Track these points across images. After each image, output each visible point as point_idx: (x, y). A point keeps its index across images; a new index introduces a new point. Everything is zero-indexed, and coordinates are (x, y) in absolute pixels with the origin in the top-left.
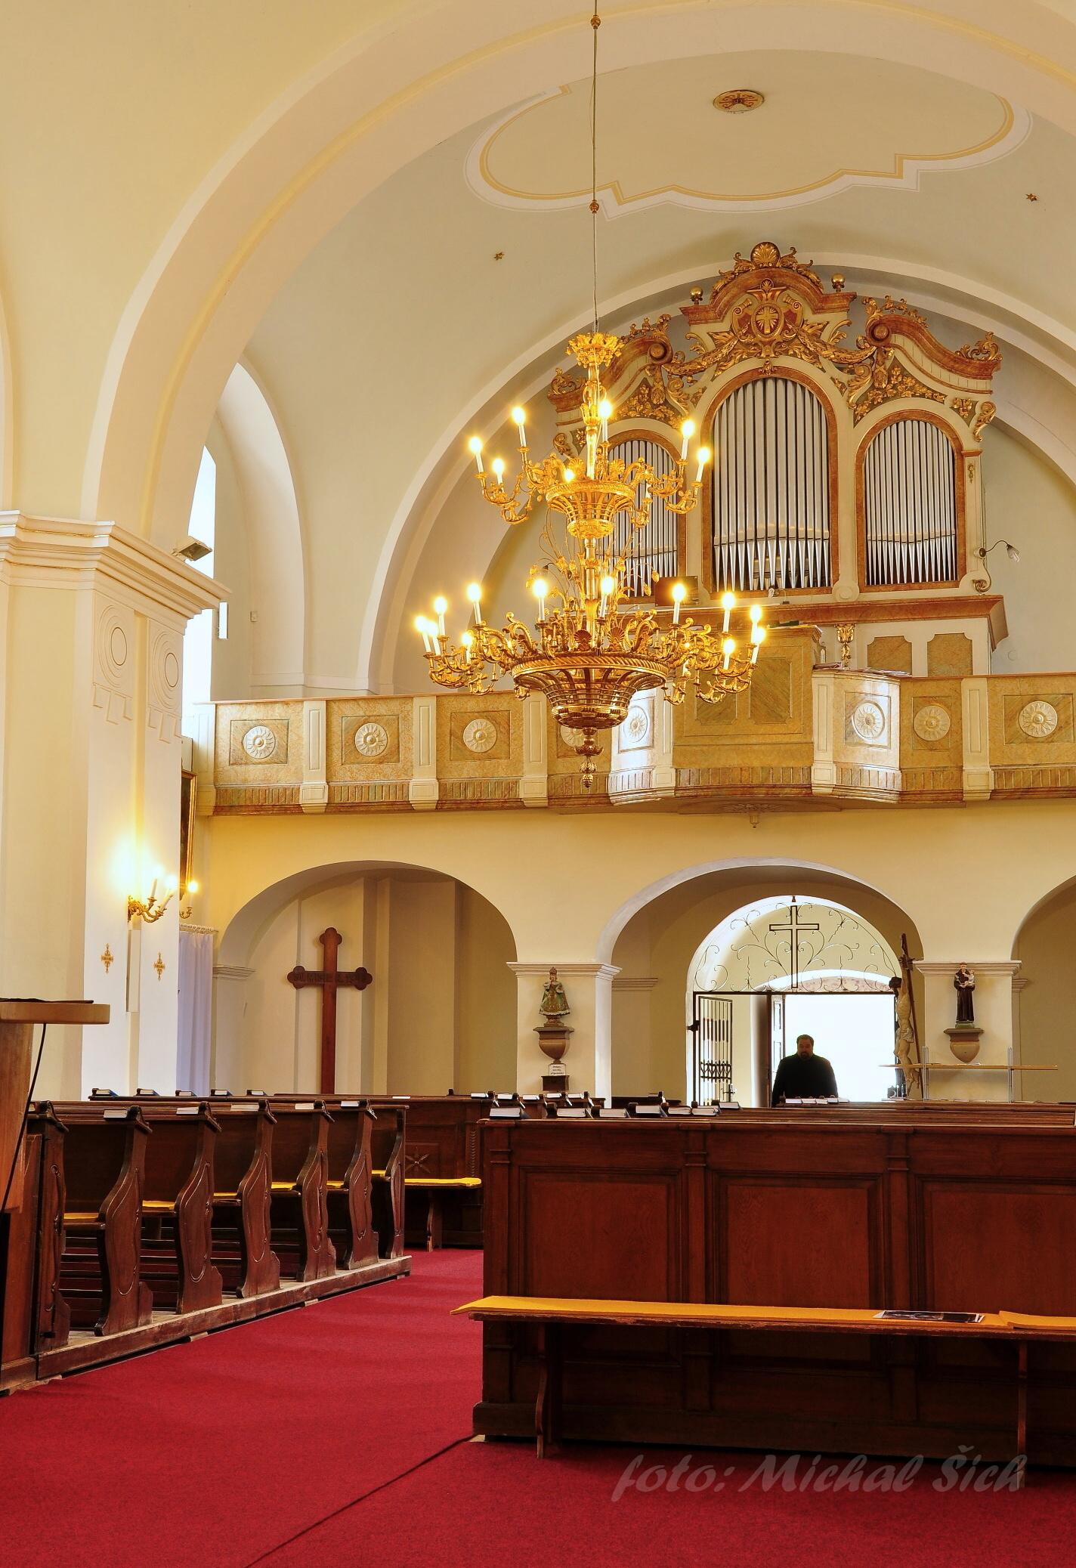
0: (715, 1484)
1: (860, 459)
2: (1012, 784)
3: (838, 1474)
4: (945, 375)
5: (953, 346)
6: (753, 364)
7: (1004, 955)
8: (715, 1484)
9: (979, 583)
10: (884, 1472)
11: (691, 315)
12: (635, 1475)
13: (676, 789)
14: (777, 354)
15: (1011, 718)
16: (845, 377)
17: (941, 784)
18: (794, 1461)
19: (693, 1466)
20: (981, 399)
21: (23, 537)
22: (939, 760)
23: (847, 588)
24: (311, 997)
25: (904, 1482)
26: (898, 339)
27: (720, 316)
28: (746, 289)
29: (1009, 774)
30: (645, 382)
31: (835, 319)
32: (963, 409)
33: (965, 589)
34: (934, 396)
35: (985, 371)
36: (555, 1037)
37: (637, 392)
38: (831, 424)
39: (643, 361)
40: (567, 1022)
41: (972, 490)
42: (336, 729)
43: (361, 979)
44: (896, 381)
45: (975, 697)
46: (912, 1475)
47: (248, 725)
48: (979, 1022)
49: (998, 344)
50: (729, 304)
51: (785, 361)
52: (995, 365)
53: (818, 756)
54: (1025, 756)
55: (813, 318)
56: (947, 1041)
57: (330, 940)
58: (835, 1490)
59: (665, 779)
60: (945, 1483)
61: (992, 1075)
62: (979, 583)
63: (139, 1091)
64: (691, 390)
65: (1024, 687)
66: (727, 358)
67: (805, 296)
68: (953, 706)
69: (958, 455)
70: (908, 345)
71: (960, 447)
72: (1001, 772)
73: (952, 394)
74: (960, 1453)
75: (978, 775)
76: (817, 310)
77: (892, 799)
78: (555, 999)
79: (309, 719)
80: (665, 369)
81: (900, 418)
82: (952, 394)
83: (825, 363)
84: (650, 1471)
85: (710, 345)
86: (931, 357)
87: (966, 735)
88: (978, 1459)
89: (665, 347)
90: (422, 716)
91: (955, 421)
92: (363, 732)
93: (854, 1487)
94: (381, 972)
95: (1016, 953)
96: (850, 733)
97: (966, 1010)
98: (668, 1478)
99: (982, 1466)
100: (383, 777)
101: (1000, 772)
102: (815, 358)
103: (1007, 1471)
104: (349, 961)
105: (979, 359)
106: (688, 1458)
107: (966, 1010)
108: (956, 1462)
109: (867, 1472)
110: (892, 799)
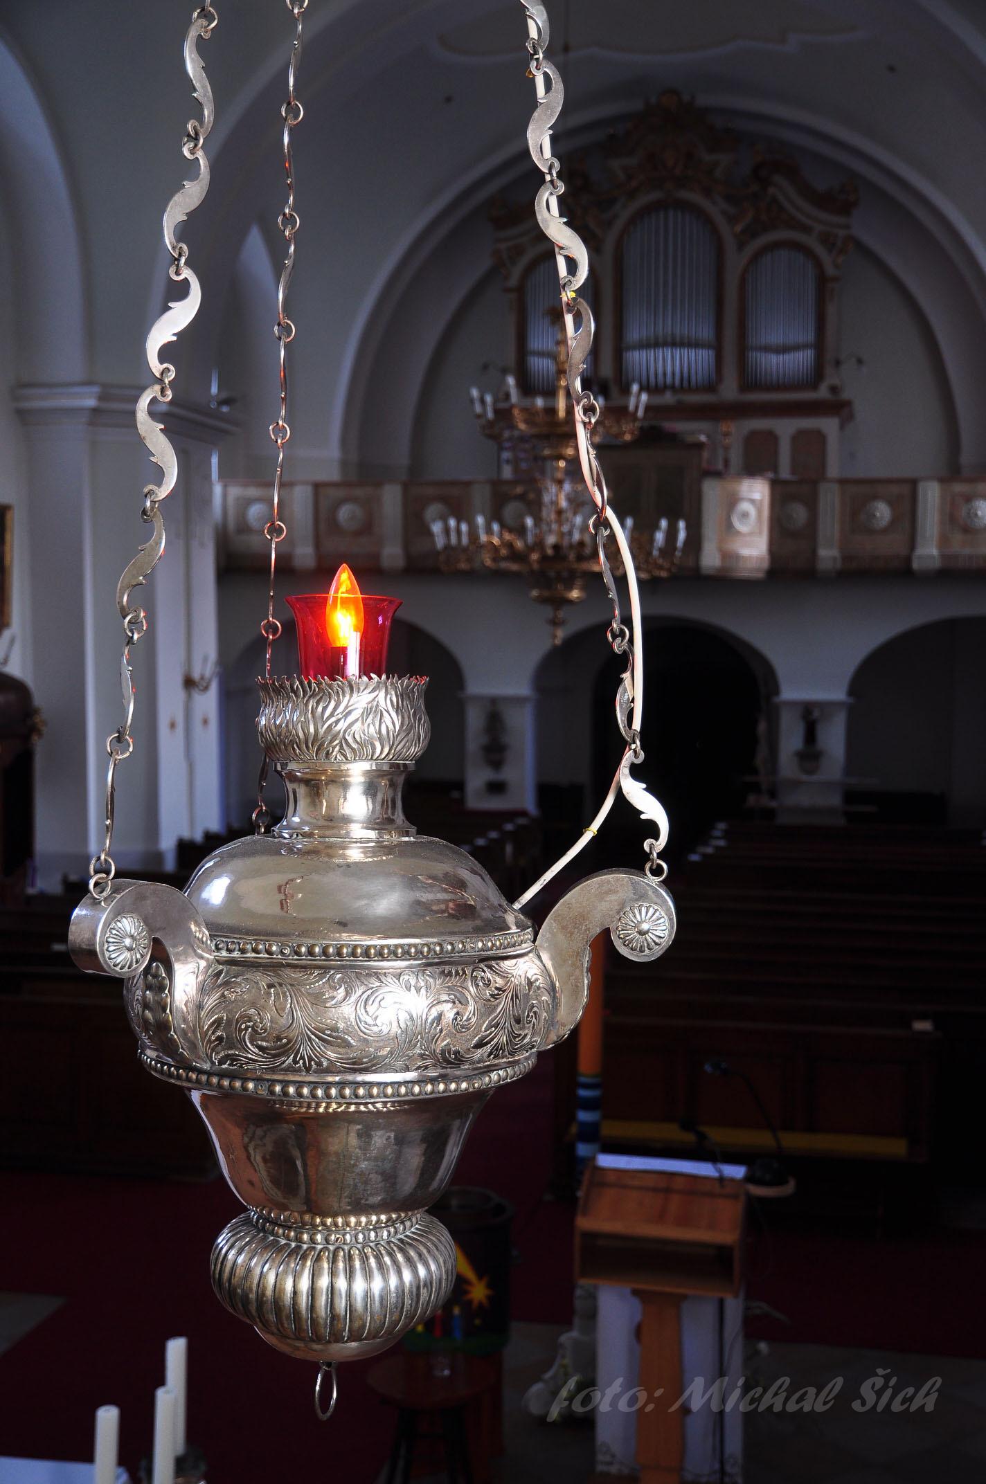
3: (765, 1391)
6: (655, 196)
9: (834, 389)
10: (806, 1393)
21: (105, 405)
25: (825, 1403)
32: (827, 240)
33: (823, 393)
36: (495, 752)
41: (831, 310)
45: (830, 500)
47: (249, 502)
51: (686, 195)
60: (863, 1403)
62: (834, 389)
68: (812, 504)
72: (846, 558)
75: (828, 554)
78: (494, 722)
79: (301, 497)
88: (893, 1381)
90: (391, 499)
91: (820, 250)
93: (777, 1408)
95: (851, 692)
96: (730, 526)
100: (890, 546)
105: (842, 198)
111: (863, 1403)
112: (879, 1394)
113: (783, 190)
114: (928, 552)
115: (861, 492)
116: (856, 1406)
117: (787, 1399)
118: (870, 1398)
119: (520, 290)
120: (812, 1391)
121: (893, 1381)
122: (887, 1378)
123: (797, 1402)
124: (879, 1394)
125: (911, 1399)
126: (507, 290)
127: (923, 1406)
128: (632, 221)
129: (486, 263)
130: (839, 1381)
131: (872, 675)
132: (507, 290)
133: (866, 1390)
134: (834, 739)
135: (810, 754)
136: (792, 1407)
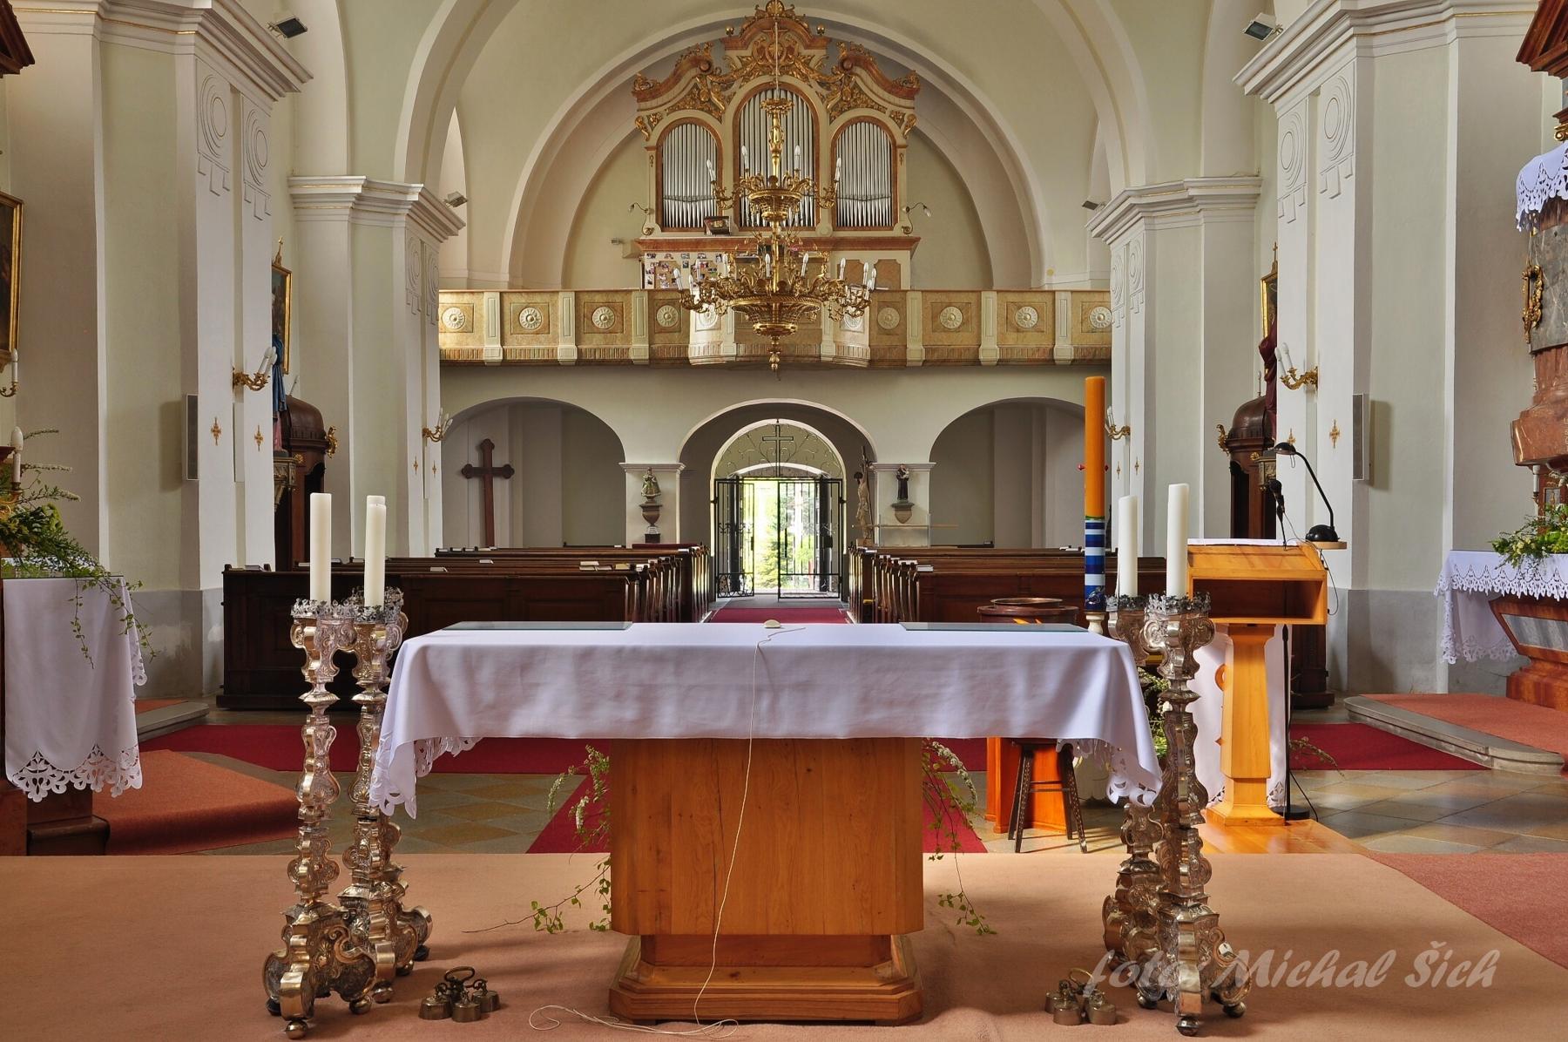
1: (834, 145)
2: (935, 357)
3: (1311, 968)
4: (886, 95)
5: (891, 77)
6: (765, 79)
7: (925, 459)
10: (1356, 968)
11: (728, 43)
14: (782, 73)
15: (935, 317)
16: (824, 92)
17: (894, 355)
18: (1267, 956)
20: (908, 112)
22: (895, 341)
23: (824, 228)
24: (474, 485)
25: (1377, 978)
26: (858, 70)
27: (745, 46)
28: (762, 29)
29: (934, 351)
30: (696, 86)
31: (818, 54)
32: (897, 118)
33: (897, 232)
34: (881, 109)
35: (910, 95)
37: (691, 92)
38: (815, 121)
39: (694, 72)
40: (659, 501)
42: (506, 311)
43: (507, 472)
44: (854, 97)
48: (910, 500)
49: (919, 79)
50: (751, 38)
52: (917, 91)
53: (825, 338)
54: (943, 340)
55: (805, 52)
56: (892, 512)
57: (486, 448)
59: (729, 349)
60: (1417, 978)
61: (921, 532)
64: (727, 93)
65: (943, 298)
66: (750, 74)
67: (800, 37)
68: (901, 308)
69: (894, 147)
70: (864, 73)
71: (894, 142)
72: (929, 350)
73: (890, 108)
74: (1431, 948)
76: (807, 47)
77: (865, 364)
78: (653, 487)
80: (710, 78)
81: (859, 120)
82: (890, 108)
83: (813, 82)
85: (739, 65)
86: (878, 83)
87: (909, 326)
88: (1449, 954)
89: (710, 64)
91: (891, 124)
92: (524, 314)
93: (1326, 983)
94: (518, 468)
97: (903, 492)
99: (1453, 963)
100: (964, 340)
101: (929, 350)
102: (805, 78)
104: (498, 460)
105: (906, 85)
107: (903, 492)
109: (1340, 966)
110: (865, 364)
111: (1417, 978)
112: (1434, 967)
113: (863, 79)
114: (990, 350)
115: (937, 301)
116: (1410, 980)
118: (1425, 972)
119: (659, 148)
120: (1363, 965)
122: (1442, 952)
123: (1348, 976)
124: (1434, 967)
125: (1468, 973)
126: (648, 148)
128: (747, 98)
129: (632, 125)
130: (1392, 954)
131: (949, 444)
132: (648, 148)
133: (1420, 963)
134: (921, 495)
135: (903, 505)
136: (1342, 982)
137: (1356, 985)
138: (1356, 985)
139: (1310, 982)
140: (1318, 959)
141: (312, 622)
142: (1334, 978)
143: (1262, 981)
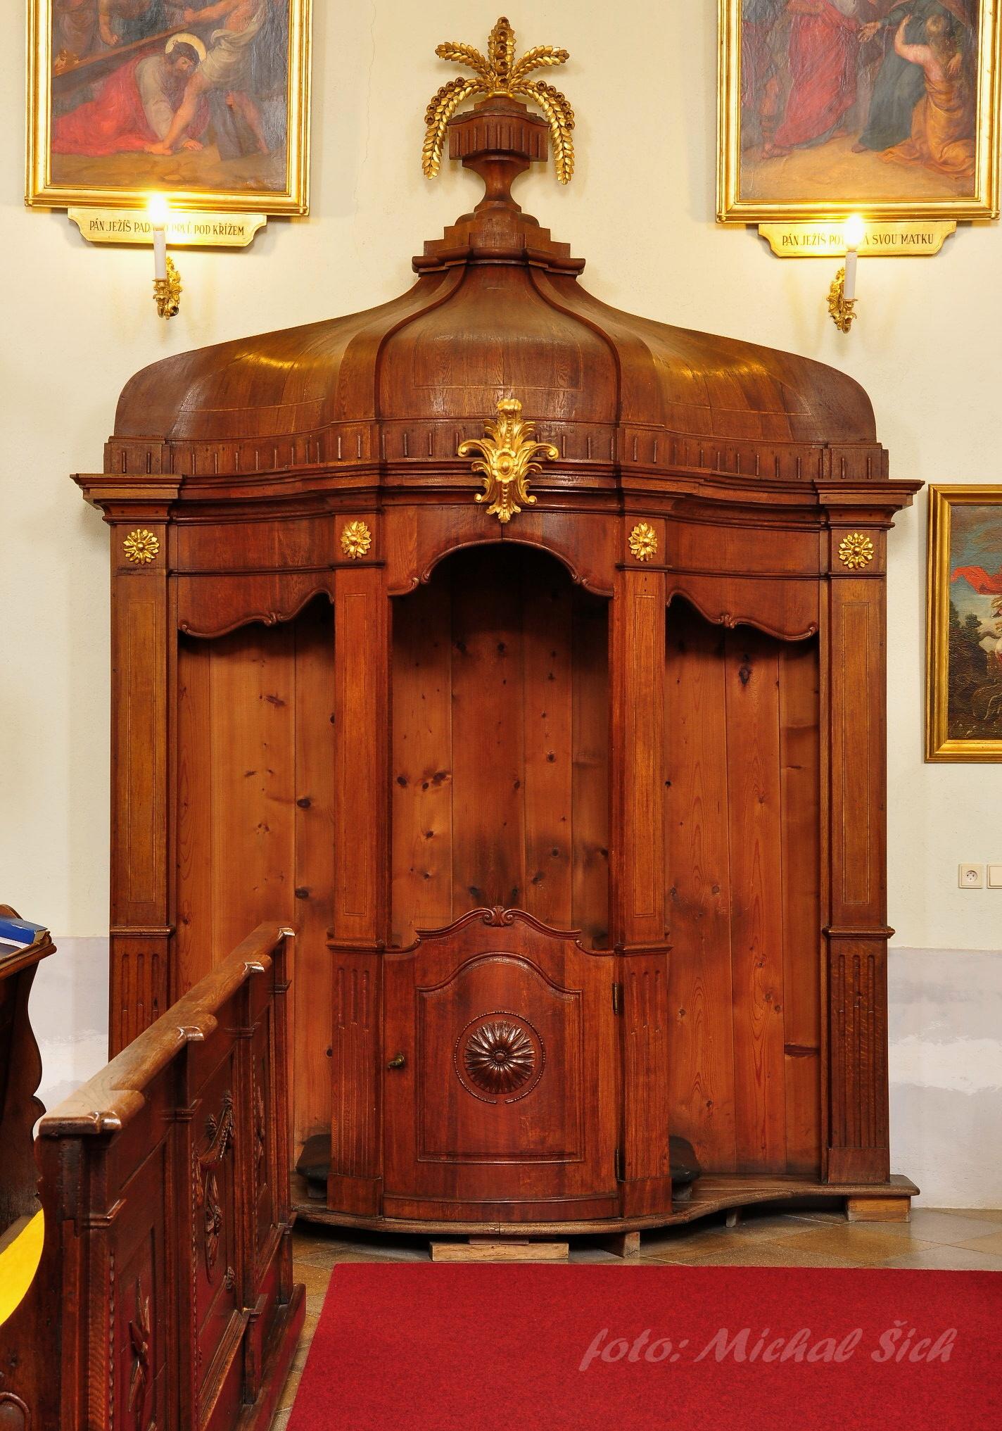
0: (672, 1353)
3: (932, 1344)
8: (672, 1353)
10: (825, 1345)
12: (601, 1347)
13: (828, 527)
18: (744, 1334)
19: (652, 1339)
46: (853, 1345)
58: (929, 1360)
60: (882, 1355)
63: (503, 31)
74: (895, 1327)
84: (613, 1343)
88: (912, 1333)
93: (799, 1358)
98: (630, 1349)
99: (914, 1341)
103: (794, 1342)
106: (647, 1332)
108: (892, 1337)
111: (882, 1355)
112: (898, 1344)
116: (875, 1356)
117: (910, 1349)
118: (889, 1349)
120: (832, 1342)
121: (912, 1333)
122: (905, 1330)
123: (818, 1353)
124: (898, 1344)
125: (928, 1349)
127: (940, 1356)
130: (859, 1332)
133: (884, 1340)
136: (813, 1357)
137: (826, 1360)
138: (826, 1360)
139: (931, 1357)
140: (843, 1338)
141: (509, 431)
142: (806, 1354)
143: (740, 1357)
